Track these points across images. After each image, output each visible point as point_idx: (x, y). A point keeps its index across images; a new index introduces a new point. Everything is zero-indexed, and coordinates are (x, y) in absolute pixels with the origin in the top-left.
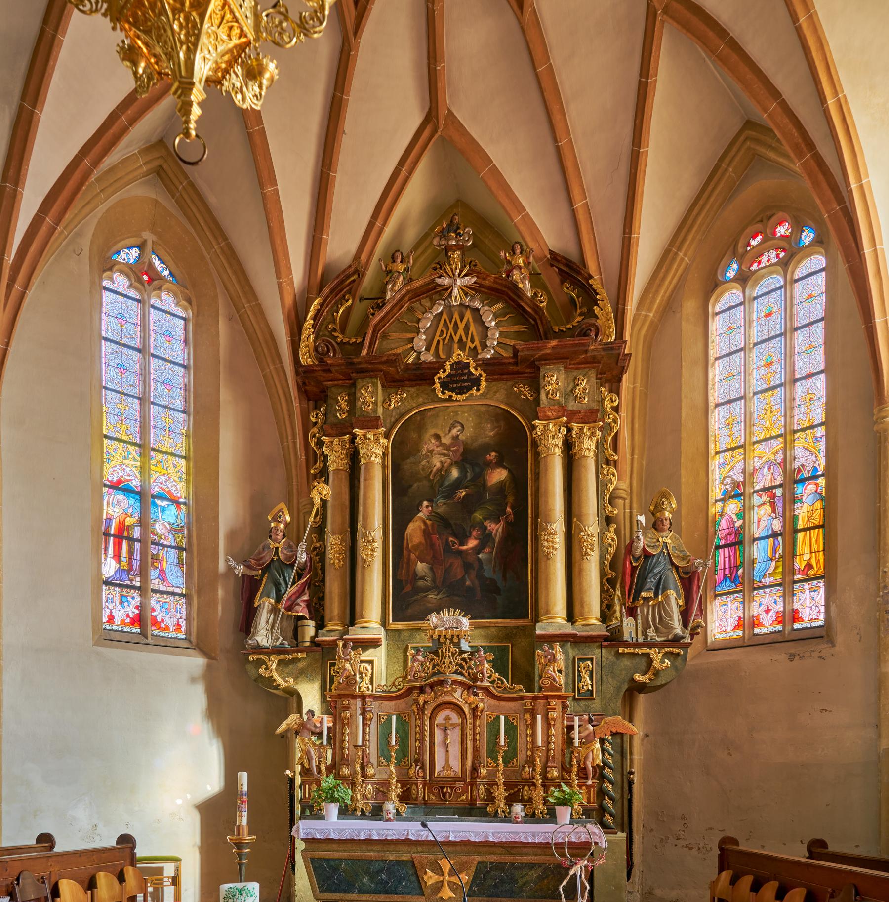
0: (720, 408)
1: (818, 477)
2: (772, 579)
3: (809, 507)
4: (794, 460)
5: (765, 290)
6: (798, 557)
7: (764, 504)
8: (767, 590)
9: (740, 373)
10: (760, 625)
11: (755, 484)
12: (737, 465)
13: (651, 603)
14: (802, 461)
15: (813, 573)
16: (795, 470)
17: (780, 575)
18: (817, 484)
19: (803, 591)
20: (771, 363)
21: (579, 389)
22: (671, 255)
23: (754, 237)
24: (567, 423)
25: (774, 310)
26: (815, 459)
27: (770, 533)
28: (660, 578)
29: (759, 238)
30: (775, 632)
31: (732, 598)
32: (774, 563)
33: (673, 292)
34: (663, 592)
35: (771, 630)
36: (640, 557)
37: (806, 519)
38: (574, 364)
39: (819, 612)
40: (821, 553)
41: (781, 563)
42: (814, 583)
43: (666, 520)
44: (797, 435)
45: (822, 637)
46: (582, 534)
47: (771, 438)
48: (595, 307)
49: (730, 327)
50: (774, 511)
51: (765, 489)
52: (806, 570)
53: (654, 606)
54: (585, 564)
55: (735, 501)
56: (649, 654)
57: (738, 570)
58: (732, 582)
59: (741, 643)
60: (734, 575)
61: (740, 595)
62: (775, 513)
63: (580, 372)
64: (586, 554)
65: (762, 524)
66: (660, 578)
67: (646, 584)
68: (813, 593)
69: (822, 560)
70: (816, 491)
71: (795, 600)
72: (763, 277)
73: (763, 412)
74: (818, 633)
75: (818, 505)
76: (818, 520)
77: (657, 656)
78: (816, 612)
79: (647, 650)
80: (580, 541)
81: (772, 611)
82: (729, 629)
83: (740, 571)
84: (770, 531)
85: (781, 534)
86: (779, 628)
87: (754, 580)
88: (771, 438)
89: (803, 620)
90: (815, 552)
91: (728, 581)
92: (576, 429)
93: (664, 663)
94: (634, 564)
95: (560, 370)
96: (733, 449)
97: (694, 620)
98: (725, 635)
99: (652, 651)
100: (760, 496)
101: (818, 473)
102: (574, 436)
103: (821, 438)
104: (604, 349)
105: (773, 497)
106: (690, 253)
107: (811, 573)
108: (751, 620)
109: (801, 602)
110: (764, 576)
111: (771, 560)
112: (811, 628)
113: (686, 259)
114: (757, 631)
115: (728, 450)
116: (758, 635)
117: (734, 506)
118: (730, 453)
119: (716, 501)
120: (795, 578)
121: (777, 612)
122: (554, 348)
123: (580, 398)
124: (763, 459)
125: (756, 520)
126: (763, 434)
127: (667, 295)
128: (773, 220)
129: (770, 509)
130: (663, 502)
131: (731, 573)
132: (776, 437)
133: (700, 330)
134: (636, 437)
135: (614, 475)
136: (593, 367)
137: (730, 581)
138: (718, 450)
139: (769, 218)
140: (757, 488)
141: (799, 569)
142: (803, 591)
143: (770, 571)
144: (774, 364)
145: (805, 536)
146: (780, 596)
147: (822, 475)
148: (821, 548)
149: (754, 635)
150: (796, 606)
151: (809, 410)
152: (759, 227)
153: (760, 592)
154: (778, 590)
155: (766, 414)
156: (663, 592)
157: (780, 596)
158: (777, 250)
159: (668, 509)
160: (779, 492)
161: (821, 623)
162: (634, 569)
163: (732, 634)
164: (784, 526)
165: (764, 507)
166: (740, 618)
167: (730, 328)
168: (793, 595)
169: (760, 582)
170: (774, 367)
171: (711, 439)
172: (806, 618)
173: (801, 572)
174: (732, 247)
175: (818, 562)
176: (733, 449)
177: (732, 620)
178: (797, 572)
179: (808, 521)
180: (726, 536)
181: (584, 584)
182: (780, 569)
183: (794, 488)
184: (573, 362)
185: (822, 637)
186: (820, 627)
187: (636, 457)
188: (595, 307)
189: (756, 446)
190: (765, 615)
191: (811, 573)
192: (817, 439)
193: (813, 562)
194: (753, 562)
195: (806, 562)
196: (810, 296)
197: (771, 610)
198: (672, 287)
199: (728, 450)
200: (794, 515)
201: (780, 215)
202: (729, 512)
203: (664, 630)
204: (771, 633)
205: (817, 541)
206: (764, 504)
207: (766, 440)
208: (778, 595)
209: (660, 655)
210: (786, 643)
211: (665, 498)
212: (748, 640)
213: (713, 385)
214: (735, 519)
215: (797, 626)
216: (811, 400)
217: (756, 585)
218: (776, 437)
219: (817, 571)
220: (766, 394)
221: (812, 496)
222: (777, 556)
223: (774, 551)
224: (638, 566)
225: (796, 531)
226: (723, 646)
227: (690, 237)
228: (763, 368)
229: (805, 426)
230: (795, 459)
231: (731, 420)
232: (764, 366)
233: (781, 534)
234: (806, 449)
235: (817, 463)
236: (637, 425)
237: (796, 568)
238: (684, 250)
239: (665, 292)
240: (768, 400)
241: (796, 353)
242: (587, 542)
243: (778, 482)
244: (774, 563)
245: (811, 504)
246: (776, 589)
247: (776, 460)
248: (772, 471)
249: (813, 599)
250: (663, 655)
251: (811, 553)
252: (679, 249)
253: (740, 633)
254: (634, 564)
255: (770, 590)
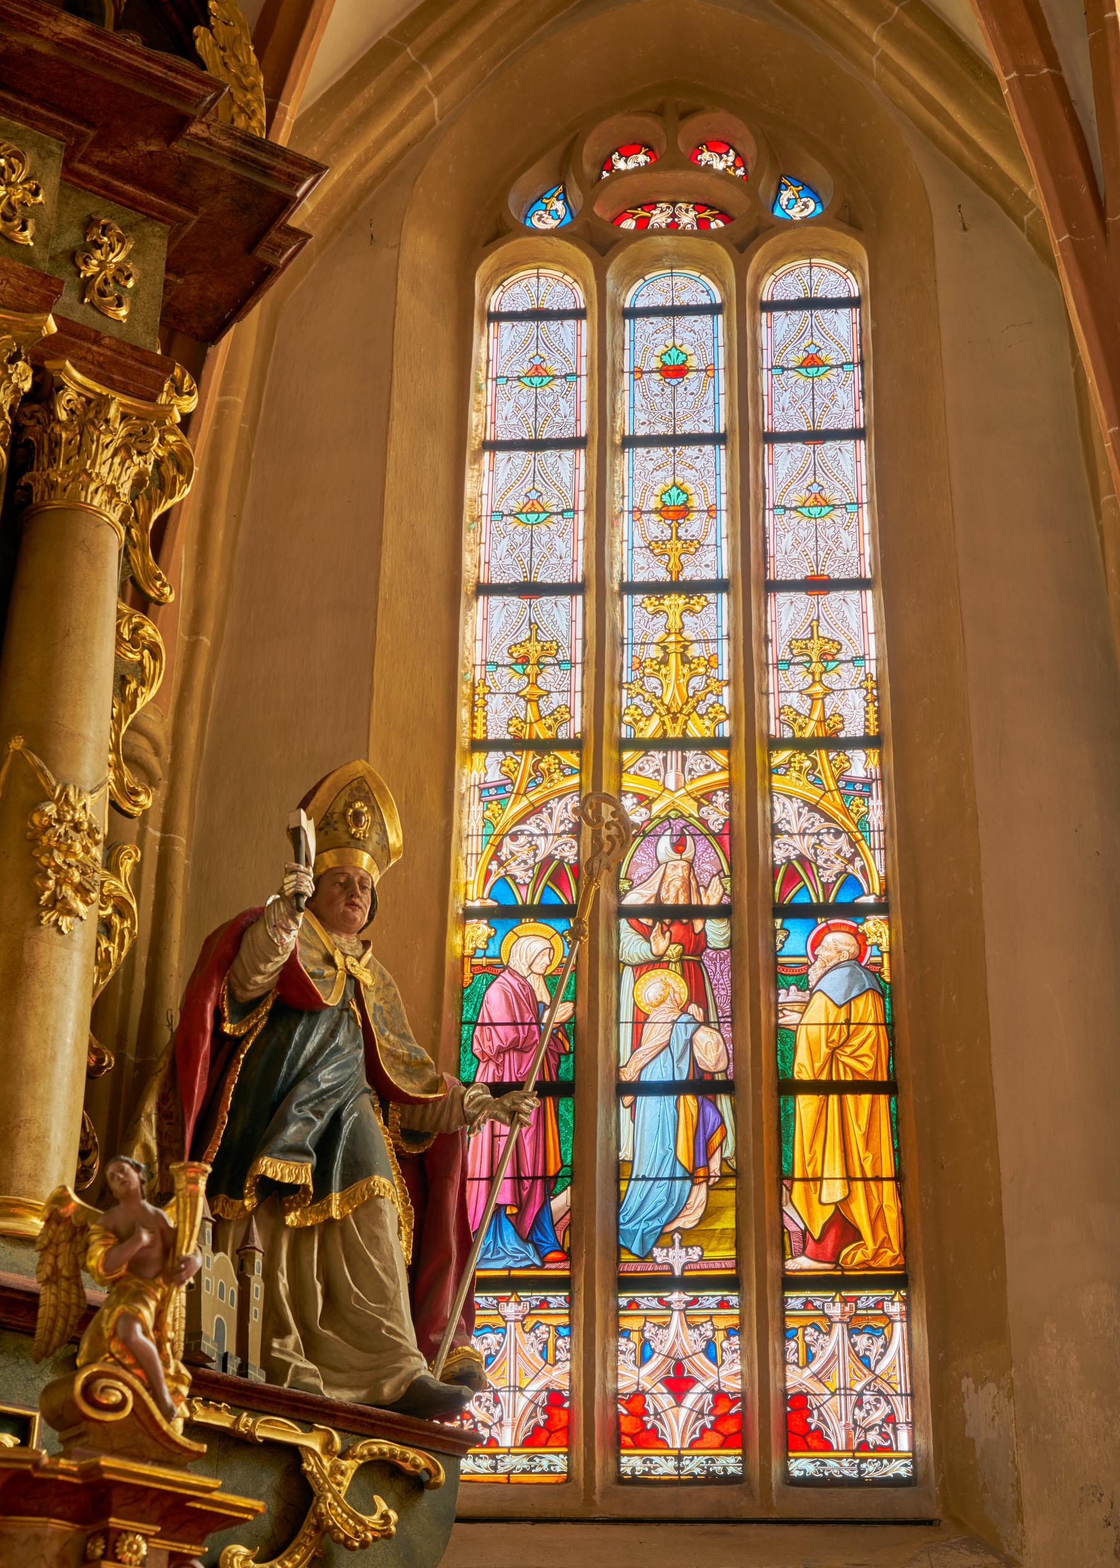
0: (496, 601)
1: (861, 912)
2: (695, 1253)
3: (833, 1010)
4: (774, 839)
5: (660, 300)
6: (798, 1187)
7: (658, 962)
8: (676, 1297)
9: (575, 511)
10: (648, 1438)
11: (624, 885)
12: (557, 806)
13: (291, 1219)
14: (803, 846)
15: (859, 1257)
16: (775, 870)
17: (729, 1244)
18: (861, 939)
19: (823, 1324)
20: (684, 511)
21: (102, 264)
22: (397, 64)
23: (626, 155)
24: (55, 347)
25: (693, 362)
26: (847, 851)
27: (683, 1073)
28: (336, 1120)
29: (642, 158)
30: (711, 1479)
31: (524, 1308)
32: (700, 1194)
33: (376, 179)
34: (346, 1182)
35: (694, 1466)
36: (257, 1002)
37: (825, 1050)
38: (98, 165)
39: (890, 1419)
40: (888, 1187)
41: (730, 1197)
42: (868, 1297)
43: (363, 888)
44: (780, 757)
45: (930, 1523)
46: (51, 809)
47: (684, 744)
48: (199, 30)
49: (537, 368)
50: (698, 995)
51: (658, 911)
52: (830, 1243)
53: (300, 1235)
54: (43, 948)
55: (542, 928)
56: (294, 1453)
57: (549, 1194)
58: (526, 1239)
59: (573, 1506)
60: (533, 1210)
61: (557, 1298)
62: (703, 1004)
63: (113, 207)
64: (58, 903)
65: (653, 1036)
66: (336, 1120)
67: (284, 1124)
68: (862, 1341)
69: (892, 1215)
70: (859, 958)
71: (791, 1358)
72: (656, 261)
73: (655, 652)
74: (906, 1504)
75: (866, 1009)
76: (870, 1062)
77: (336, 1470)
78: (877, 1416)
79: (286, 1432)
80: (34, 841)
81: (698, 1388)
82: (506, 1438)
83: (561, 1202)
84: (685, 1065)
85: (727, 1087)
86: (729, 1462)
87: (619, 1247)
88: (684, 744)
89: (828, 1447)
90: (864, 1179)
91: (508, 1231)
92: (70, 394)
93: (372, 1510)
94: (228, 1028)
95: (50, 154)
96: (542, 747)
97: (453, 1346)
98: (487, 1463)
99: (313, 1442)
100: (645, 933)
101: (863, 900)
102: (63, 415)
103: (869, 785)
104: (236, 158)
105: (697, 945)
106: (451, 90)
107: (854, 1256)
108: (611, 1413)
109: (815, 1367)
110: (662, 1238)
111: (691, 1176)
112: (859, 1483)
113: (435, 101)
114: (632, 1463)
115: (515, 744)
116: (635, 1481)
117: (539, 945)
118: (528, 758)
119: (469, 914)
120: (791, 1265)
121: (719, 1396)
122: (66, 45)
123: (102, 294)
124: (656, 808)
125: (626, 1014)
126: (656, 720)
127: (362, 177)
128: (694, 126)
129: (681, 989)
130: (357, 815)
131: (521, 1204)
132: (706, 745)
133: (445, 335)
134: (215, 575)
135: (155, 654)
136: (164, 216)
137: (518, 1231)
138: (479, 735)
139: (684, 115)
140: (633, 899)
141: (805, 1232)
142: (823, 1324)
143: (687, 1221)
144: (694, 516)
145: (822, 1111)
146: (729, 1332)
147: (881, 908)
148: (887, 1170)
149: (620, 1480)
150: (797, 1378)
151: (818, 688)
152: (649, 126)
153: (647, 1299)
154: (723, 1304)
155: (664, 662)
156: (347, 1182)
157: (729, 1332)
158: (700, 207)
159: (371, 846)
160: (716, 932)
161: (900, 1469)
162: (226, 1047)
163: (521, 1462)
164: (735, 1058)
165: (659, 974)
166: (555, 1398)
167: (537, 371)
168: (785, 1334)
169: (646, 1256)
170: (693, 526)
171: (464, 690)
172: (838, 1436)
173: (811, 1245)
174: (559, 149)
175: (877, 1218)
176: (542, 747)
177: (522, 1402)
178: (797, 1245)
179: (832, 1057)
180: (501, 1051)
181: (32, 1038)
182: (727, 1222)
183: (775, 932)
184: (99, 156)
185: (930, 1523)
186: (896, 1482)
187: (206, 641)
188: (199, 30)
189: (627, 755)
190: (666, 1400)
191: (854, 1256)
192: (848, 786)
193: (860, 1214)
194: (619, 1171)
195: (830, 1210)
196: (812, 361)
197: (692, 1381)
198: (378, 161)
199: (515, 744)
200: (778, 1026)
201: (717, 119)
202: (519, 963)
203: (355, 1357)
204: (694, 1481)
205: (868, 1137)
206: (658, 962)
207: (663, 744)
208: (721, 1323)
209: (350, 1466)
210: (786, 1529)
211: (368, 799)
212: (603, 1495)
213: (473, 520)
214: (543, 996)
215: (802, 1465)
216: (824, 657)
217: (631, 1266)
218: (706, 745)
219: (876, 1255)
220: (667, 601)
221: (846, 971)
222: (715, 1165)
223: (703, 1146)
224: (244, 1037)
225: (789, 1088)
226: (492, 1509)
227: (466, 40)
228: (655, 517)
229: (807, 734)
230: (775, 831)
231: (534, 649)
232: (656, 511)
233: (727, 1087)
234: (813, 808)
235: (858, 863)
236: (219, 534)
237: (791, 1227)
238: (440, 67)
239: (360, 165)
240: (674, 622)
241: (768, 505)
242: (69, 851)
243: (713, 896)
244: (700, 1194)
245: (840, 1001)
246: (710, 1298)
247: (703, 822)
248: (688, 854)
249: (864, 1360)
250: (360, 1468)
251: (849, 1179)
252: (429, 56)
253: (553, 1461)
254: (228, 1028)
255: (687, 1297)
